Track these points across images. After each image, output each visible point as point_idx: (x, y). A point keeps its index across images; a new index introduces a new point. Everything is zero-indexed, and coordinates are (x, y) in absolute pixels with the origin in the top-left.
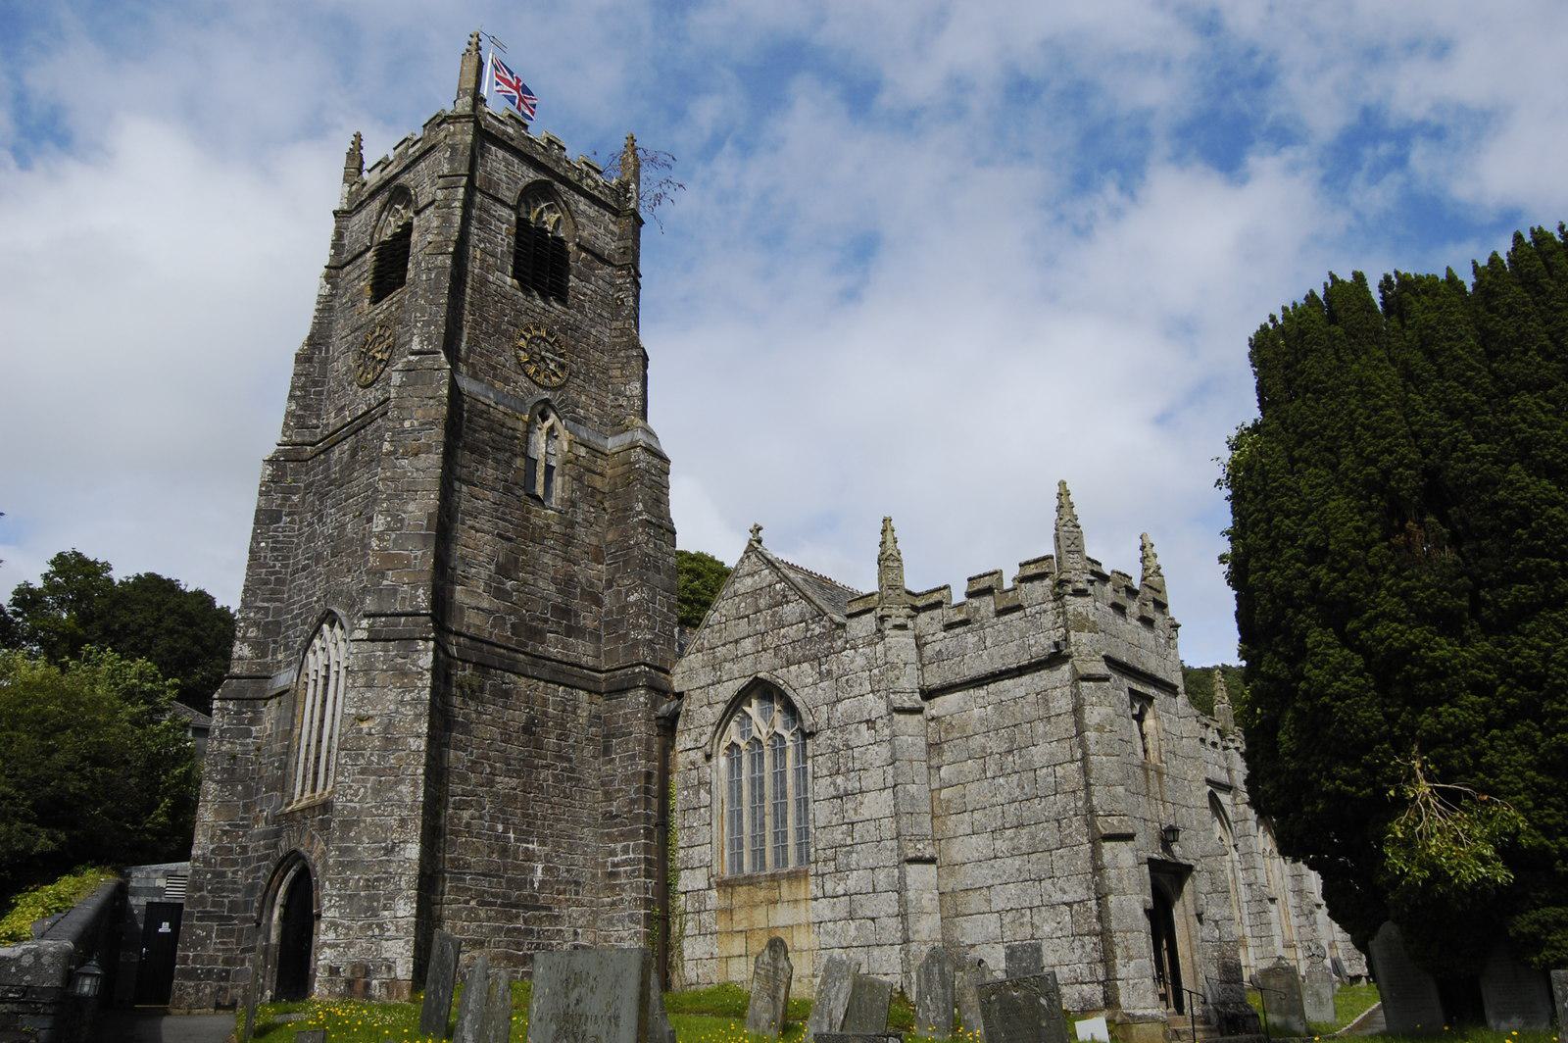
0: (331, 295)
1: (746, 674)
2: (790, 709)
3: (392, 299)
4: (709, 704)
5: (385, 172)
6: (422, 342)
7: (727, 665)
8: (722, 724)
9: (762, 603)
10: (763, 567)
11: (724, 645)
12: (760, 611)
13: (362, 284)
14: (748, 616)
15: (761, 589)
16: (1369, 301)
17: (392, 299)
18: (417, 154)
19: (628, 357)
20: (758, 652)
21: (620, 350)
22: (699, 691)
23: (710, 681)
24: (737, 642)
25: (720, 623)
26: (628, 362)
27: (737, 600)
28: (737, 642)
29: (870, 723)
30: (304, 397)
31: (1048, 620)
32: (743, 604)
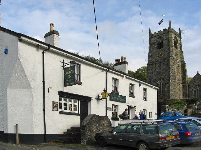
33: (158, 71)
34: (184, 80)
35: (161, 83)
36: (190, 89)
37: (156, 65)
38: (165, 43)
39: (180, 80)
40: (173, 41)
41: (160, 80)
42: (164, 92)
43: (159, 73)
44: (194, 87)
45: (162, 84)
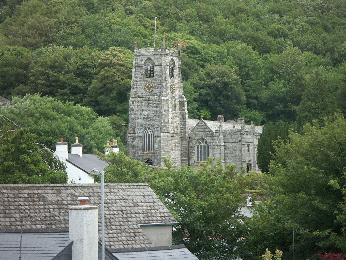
2: (206, 142)
8: (196, 142)
9: (203, 128)
29: (218, 146)
31: (239, 137)
33: (146, 113)
34: (182, 128)
35: (149, 134)
36: (191, 143)
37: (143, 103)
38: (157, 69)
39: (177, 129)
40: (168, 67)
41: (149, 129)
42: (154, 150)
43: (147, 118)
44: (197, 141)
45: (148, 135)
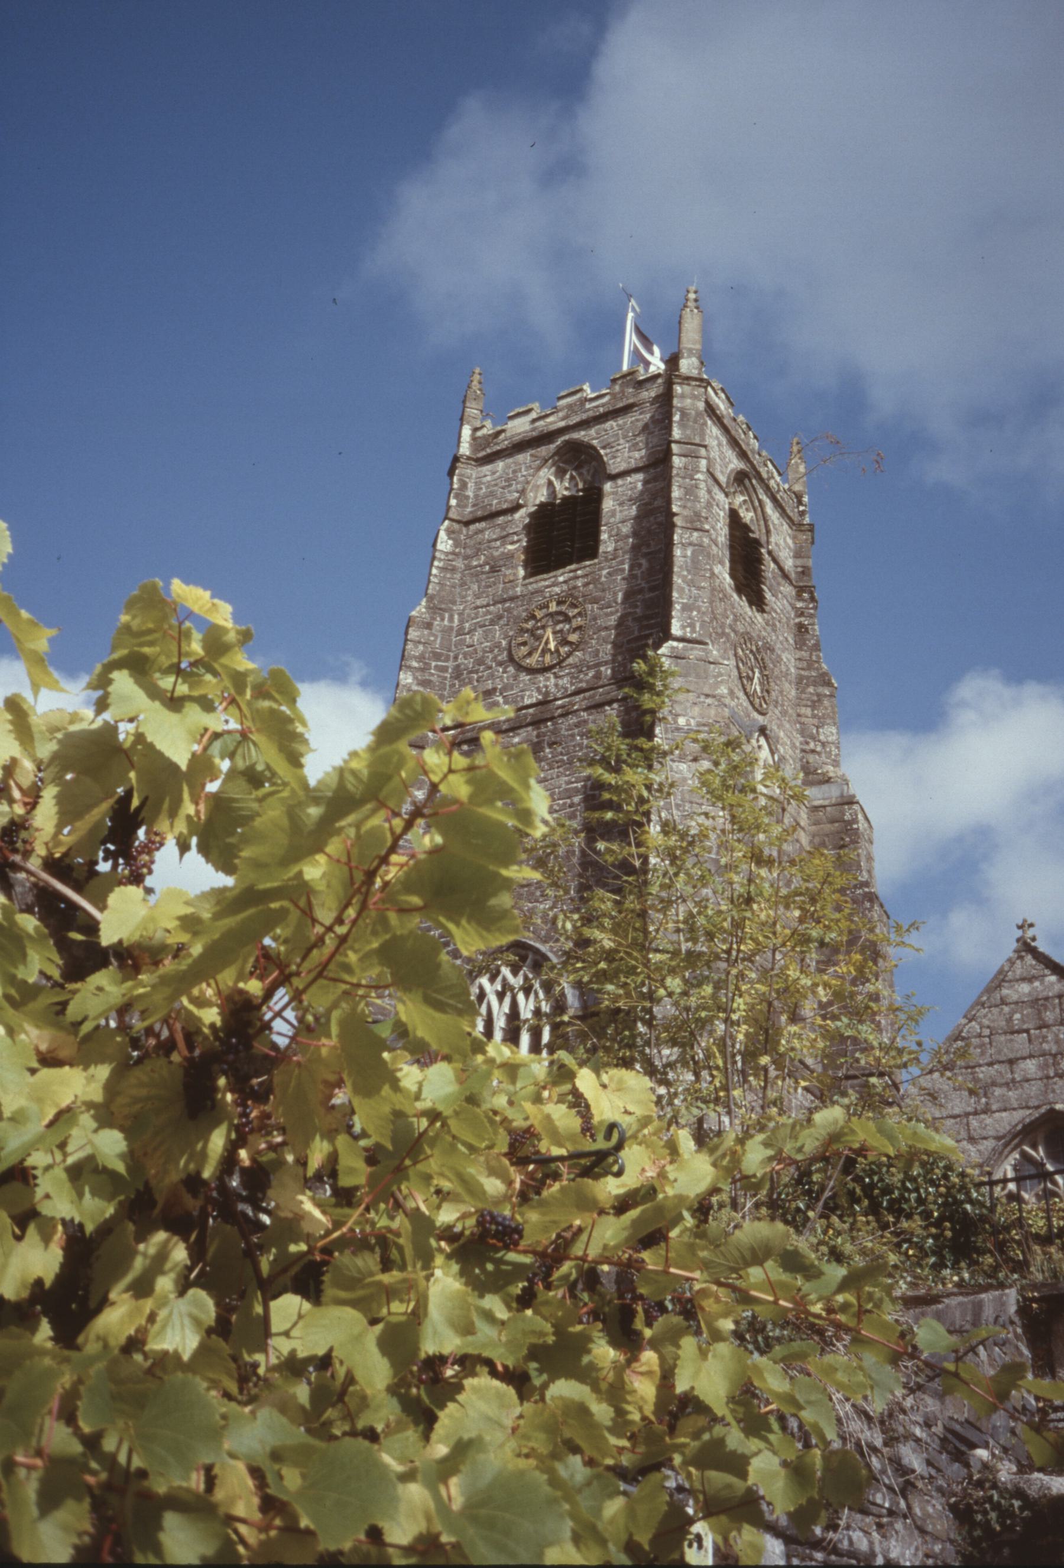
0: (453, 553)
1: (1031, 1104)
3: (575, 571)
4: (972, 1140)
5: (541, 423)
6: (683, 627)
7: (998, 1091)
10: (1048, 972)
11: (990, 1064)
12: (1047, 1026)
13: (510, 547)
14: (1027, 1031)
15: (1047, 999)
16: (81, 942)
17: (575, 571)
18: (601, 410)
19: (818, 695)
20: (1048, 1077)
21: (808, 685)
22: (953, 1121)
23: (970, 1109)
24: (1011, 1062)
25: (980, 1036)
26: (819, 701)
27: (1006, 1009)
28: (1011, 1062)
30: (422, 670)
32: (1017, 1016)
